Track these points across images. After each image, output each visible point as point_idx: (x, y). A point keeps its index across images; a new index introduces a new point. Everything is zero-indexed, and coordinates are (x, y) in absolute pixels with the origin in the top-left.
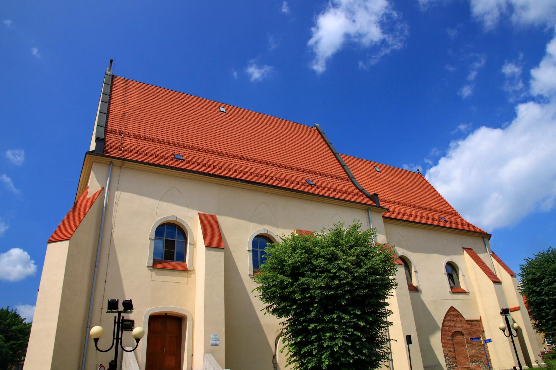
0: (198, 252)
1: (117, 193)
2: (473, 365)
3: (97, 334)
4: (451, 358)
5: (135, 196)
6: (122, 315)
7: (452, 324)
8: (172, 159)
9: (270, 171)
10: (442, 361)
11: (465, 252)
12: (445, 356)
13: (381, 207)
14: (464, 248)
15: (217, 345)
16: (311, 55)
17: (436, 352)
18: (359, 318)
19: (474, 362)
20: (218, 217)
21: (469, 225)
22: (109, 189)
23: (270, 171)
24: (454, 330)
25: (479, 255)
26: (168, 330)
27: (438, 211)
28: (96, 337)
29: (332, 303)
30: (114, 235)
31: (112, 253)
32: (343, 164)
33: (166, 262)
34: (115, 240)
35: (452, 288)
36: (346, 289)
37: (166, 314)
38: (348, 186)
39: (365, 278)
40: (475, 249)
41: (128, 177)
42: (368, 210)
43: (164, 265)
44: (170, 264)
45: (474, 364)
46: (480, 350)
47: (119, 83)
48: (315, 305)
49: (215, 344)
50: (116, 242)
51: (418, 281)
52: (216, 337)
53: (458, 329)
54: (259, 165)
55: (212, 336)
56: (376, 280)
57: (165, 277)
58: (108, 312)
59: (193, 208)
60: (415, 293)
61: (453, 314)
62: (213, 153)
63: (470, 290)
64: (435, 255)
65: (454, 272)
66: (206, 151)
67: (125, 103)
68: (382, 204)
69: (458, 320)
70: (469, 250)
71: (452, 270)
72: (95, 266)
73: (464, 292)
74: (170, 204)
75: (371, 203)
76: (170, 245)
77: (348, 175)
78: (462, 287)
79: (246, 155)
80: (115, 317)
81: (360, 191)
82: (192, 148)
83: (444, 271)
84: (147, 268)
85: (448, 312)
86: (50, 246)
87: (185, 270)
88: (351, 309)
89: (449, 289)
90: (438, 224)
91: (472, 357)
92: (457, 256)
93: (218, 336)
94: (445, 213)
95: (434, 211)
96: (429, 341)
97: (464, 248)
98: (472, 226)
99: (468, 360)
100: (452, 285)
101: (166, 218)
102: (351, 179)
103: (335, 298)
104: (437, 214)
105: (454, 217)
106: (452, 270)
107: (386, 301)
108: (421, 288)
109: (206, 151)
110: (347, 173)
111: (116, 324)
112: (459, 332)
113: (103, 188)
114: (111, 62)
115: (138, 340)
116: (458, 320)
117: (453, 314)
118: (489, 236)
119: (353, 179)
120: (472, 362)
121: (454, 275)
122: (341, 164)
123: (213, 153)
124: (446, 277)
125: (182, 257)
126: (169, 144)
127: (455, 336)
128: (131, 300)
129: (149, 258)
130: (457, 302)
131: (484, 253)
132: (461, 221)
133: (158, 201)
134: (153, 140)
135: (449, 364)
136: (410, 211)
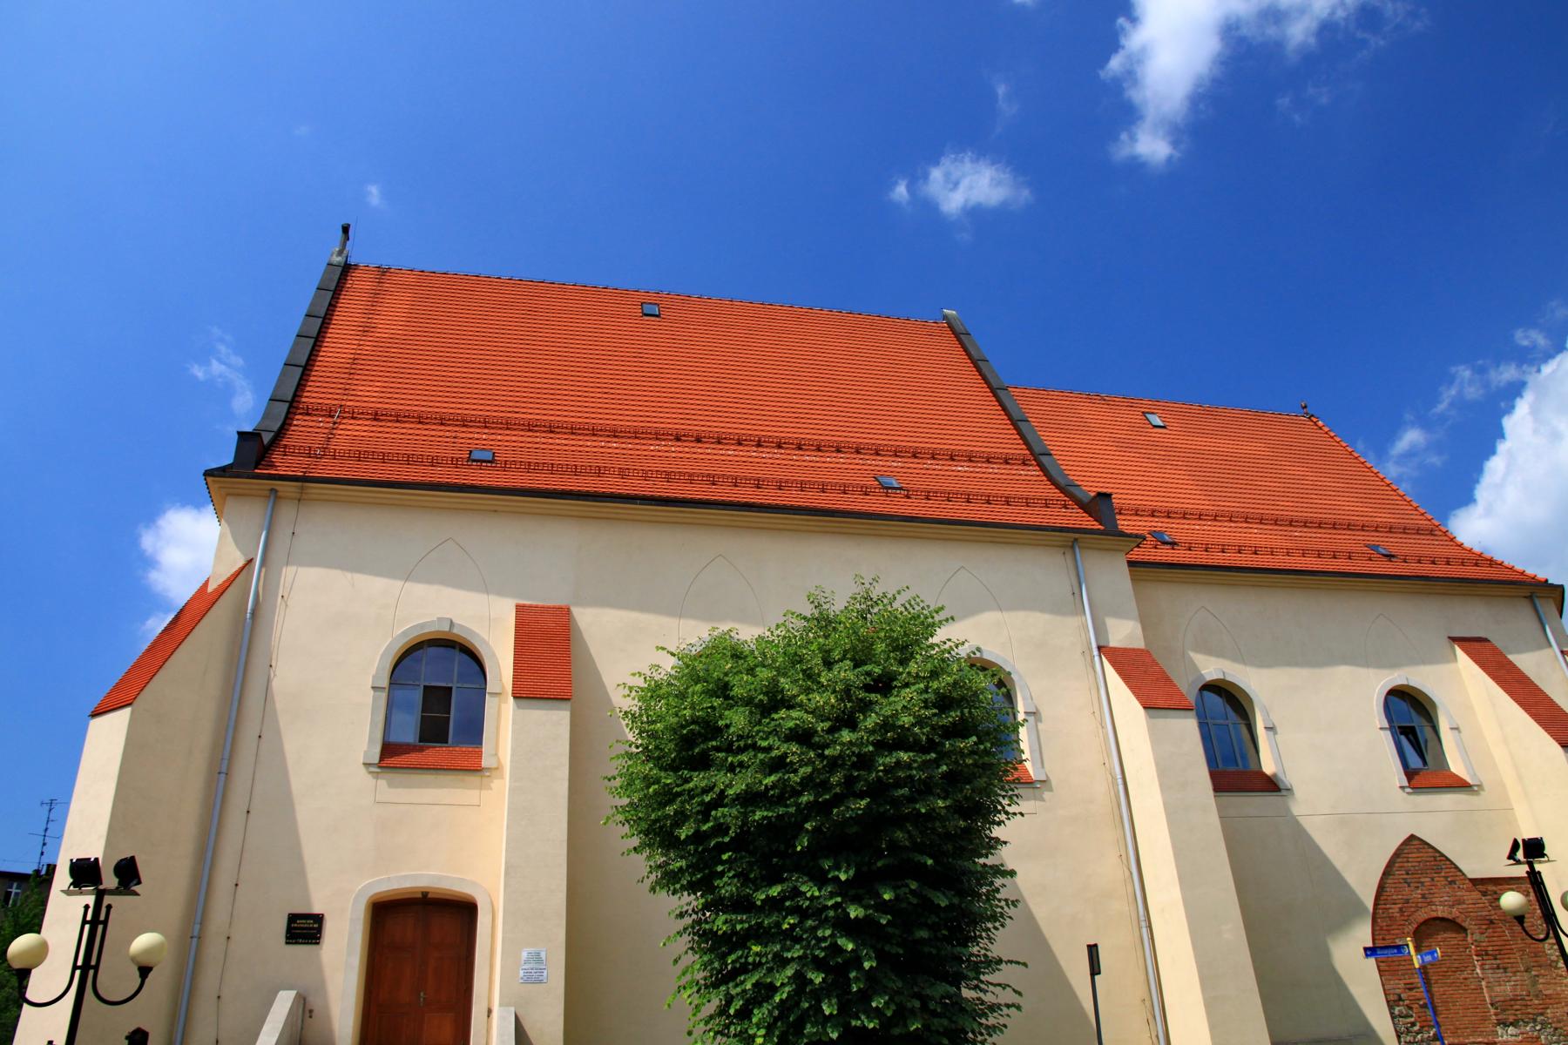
0: (505, 720)
1: (288, 572)
2: (1508, 1034)
3: (148, 951)
4: (1416, 1002)
5: (335, 574)
6: (107, 900)
7: (1417, 894)
8: (455, 462)
9: (766, 463)
10: (1380, 1019)
11: (1459, 651)
12: (1391, 1006)
13: (1122, 534)
14: (1454, 640)
15: (541, 982)
16: (1121, 111)
17: (1355, 990)
18: (850, 891)
19: (1514, 1024)
20: (577, 612)
21: (1480, 560)
22: (264, 563)
23: (766, 463)
24: (1423, 915)
25: (1511, 657)
26: (423, 939)
27: (1363, 527)
28: (145, 962)
29: (782, 847)
30: (275, 684)
31: (269, 735)
32: (1015, 416)
33: (421, 749)
34: (277, 698)
35: (1410, 774)
36: (804, 799)
37: (425, 894)
38: (1028, 480)
39: (865, 762)
40: (1498, 642)
41: (320, 524)
42: (1072, 547)
43: (413, 758)
44: (434, 753)
45: (1511, 1030)
46: (1535, 983)
47: (356, 283)
48: (725, 857)
49: (534, 979)
50: (280, 702)
51: (1278, 758)
52: (537, 958)
53: (1441, 912)
54: (731, 451)
55: (524, 955)
56: (898, 763)
57: (400, 790)
58: (67, 892)
59: (501, 592)
60: (1252, 804)
61: (1416, 861)
62: (594, 432)
63: (1484, 777)
64: (1343, 671)
65: (1424, 722)
66: (573, 430)
67: (366, 330)
68: (1124, 524)
69: (1440, 881)
70: (1477, 645)
71: (1411, 717)
72: (221, 770)
73: (1461, 785)
74: (435, 588)
75: (1089, 523)
76: (437, 698)
77: (1029, 448)
78: (1453, 769)
79: (695, 427)
80: (87, 907)
81: (1062, 490)
82: (530, 427)
83: (1379, 719)
84: (363, 770)
85: (1397, 854)
86: (95, 724)
87: (476, 769)
88: (826, 865)
89: (1399, 777)
90: (1358, 570)
91: (1503, 1005)
92: (1249, 670)
93: (543, 955)
94: (1391, 530)
95: (1349, 527)
96: (1326, 955)
97: (1454, 640)
98: (1491, 562)
99: (1485, 1019)
100: (1415, 761)
101: (422, 626)
102: (1037, 457)
103: (782, 831)
104: (1360, 536)
105: (1425, 540)
106: (1411, 717)
107: (997, 832)
108: (1290, 778)
109: (573, 430)
110: (1026, 443)
111: (87, 927)
112: (1443, 919)
113: (250, 561)
114: (346, 229)
115: (145, 971)
116: (1440, 881)
117: (1416, 861)
118: (1553, 593)
119: (1044, 459)
120: (1505, 1024)
121: (1425, 732)
122: (1007, 414)
123: (594, 432)
124: (1386, 742)
125: (474, 731)
126: (465, 423)
127: (1429, 936)
128: (133, 858)
129: (371, 740)
130: (1434, 818)
131: (1540, 648)
132: (1451, 552)
133: (399, 583)
134: (420, 420)
135: (1408, 1031)
136: (1255, 535)
